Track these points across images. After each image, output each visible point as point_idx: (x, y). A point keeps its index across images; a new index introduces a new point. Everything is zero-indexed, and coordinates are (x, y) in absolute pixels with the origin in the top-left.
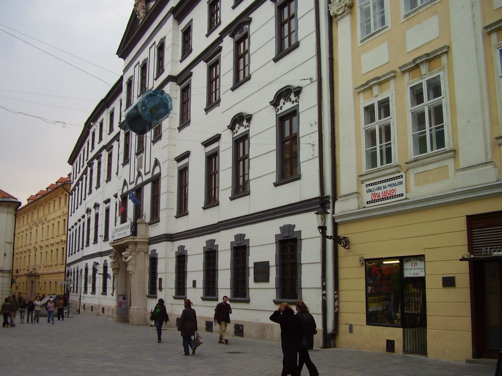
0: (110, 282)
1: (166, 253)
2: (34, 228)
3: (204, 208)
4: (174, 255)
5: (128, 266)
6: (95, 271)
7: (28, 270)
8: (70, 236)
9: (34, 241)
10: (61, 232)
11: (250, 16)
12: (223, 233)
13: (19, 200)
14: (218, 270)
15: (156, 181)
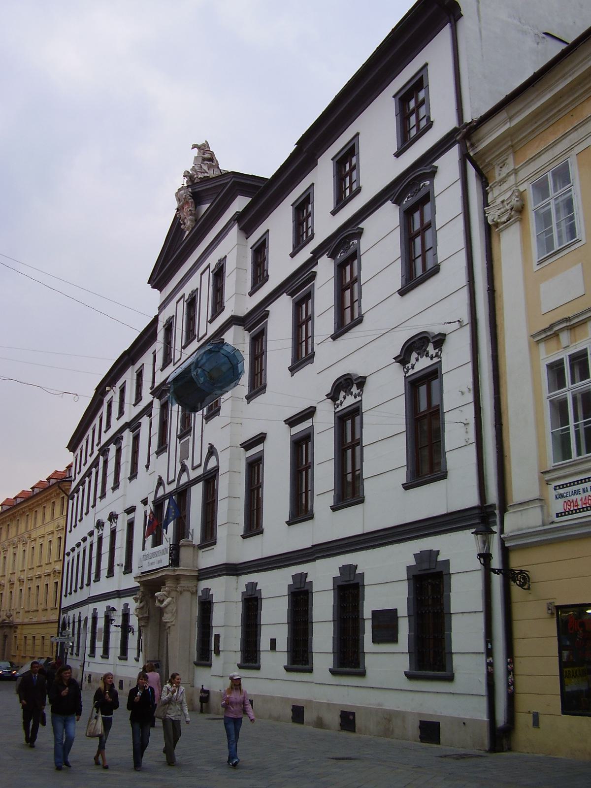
1: (227, 594)
2: (11, 550)
3: (289, 523)
4: (239, 598)
5: (165, 614)
6: (108, 620)
8: (68, 564)
10: (54, 557)
11: (360, 226)
12: (320, 563)
15: (210, 479)
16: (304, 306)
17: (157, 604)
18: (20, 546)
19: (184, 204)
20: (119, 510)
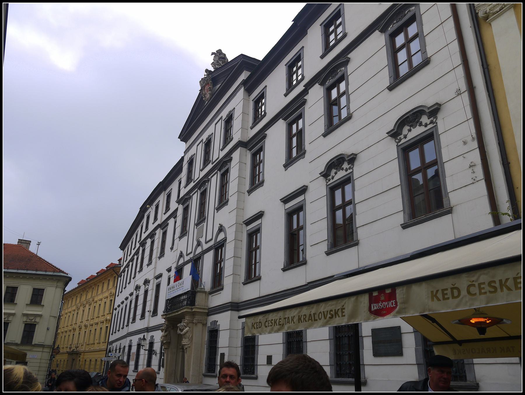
2: (82, 308)
3: (284, 270)
6: (139, 346)
7: (70, 348)
9: (79, 320)
10: (107, 311)
11: (349, 56)
14: (306, 342)
15: (219, 247)
17: (179, 332)
18: (87, 306)
19: (206, 84)
20: (150, 276)
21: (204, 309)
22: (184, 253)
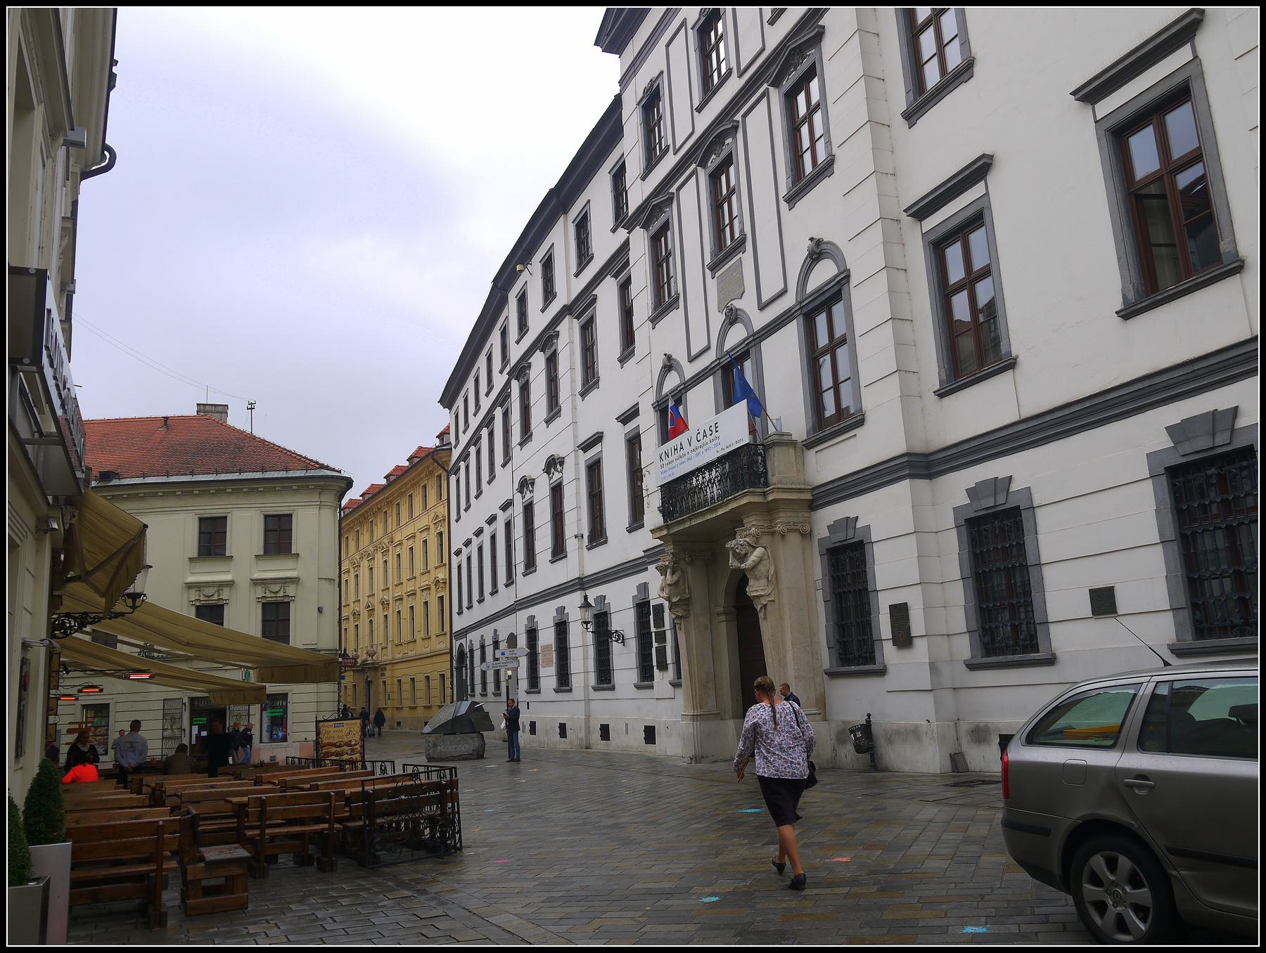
0: (624, 658)
2: (365, 564)
3: (1128, 313)
5: (751, 582)
8: (459, 567)
10: (433, 560)
13: (343, 474)
15: (821, 306)
16: (723, 178)
17: (733, 563)
18: (379, 556)
21: (800, 490)
22: (681, 356)
